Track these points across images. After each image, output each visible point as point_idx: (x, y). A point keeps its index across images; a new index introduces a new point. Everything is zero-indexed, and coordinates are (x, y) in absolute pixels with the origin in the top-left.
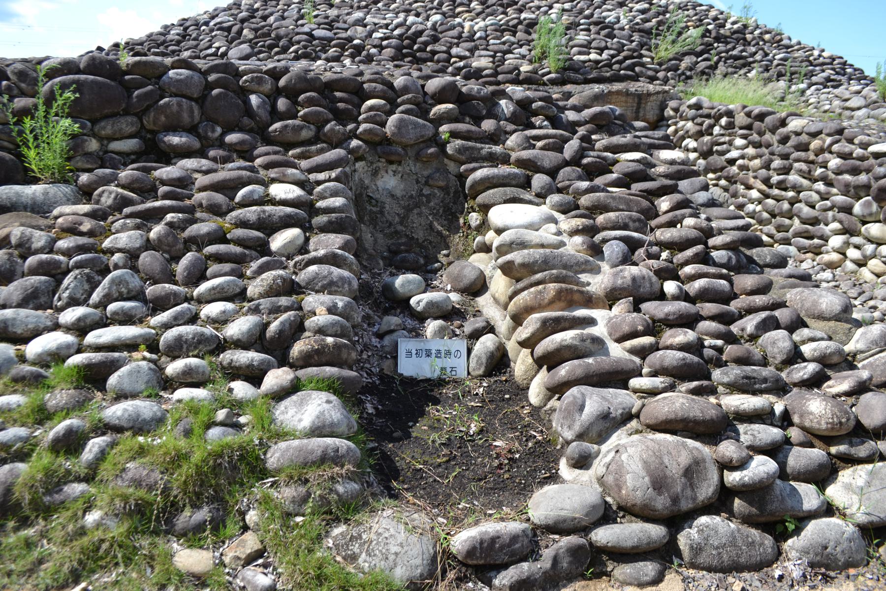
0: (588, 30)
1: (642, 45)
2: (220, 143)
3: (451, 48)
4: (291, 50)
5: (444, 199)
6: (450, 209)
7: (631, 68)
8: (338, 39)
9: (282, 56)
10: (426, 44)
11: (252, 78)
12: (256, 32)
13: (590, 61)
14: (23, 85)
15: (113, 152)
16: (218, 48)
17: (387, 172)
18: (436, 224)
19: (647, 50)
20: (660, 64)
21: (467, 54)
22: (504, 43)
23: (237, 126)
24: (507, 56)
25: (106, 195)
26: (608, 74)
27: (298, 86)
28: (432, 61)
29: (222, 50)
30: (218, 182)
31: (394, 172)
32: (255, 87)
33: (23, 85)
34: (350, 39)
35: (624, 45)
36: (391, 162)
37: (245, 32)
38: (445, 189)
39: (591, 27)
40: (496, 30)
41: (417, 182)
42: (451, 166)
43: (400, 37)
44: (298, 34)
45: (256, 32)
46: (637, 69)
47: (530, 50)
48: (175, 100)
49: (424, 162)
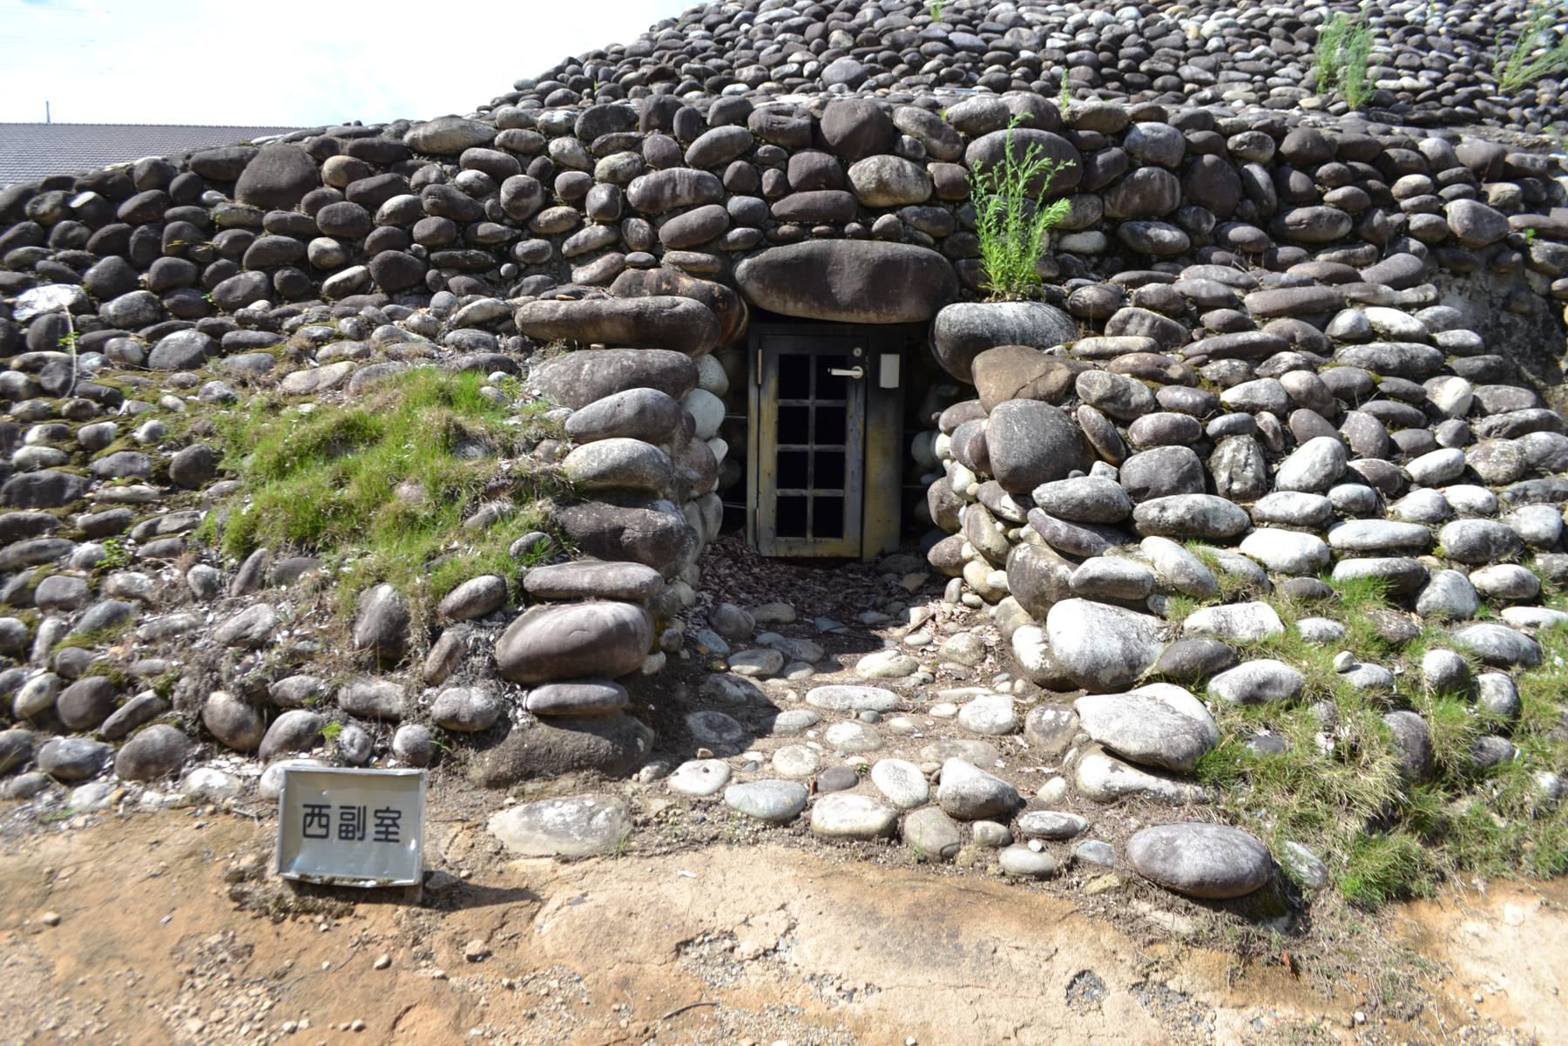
0: (1383, 35)
1: (1474, 61)
2: (1222, 242)
3: (1177, 66)
4: (927, 67)
5: (1529, 331)
6: (1541, 347)
7: (1468, 101)
8: (995, 49)
9: (914, 79)
10: (1138, 59)
11: (1252, 138)
12: (855, 36)
13: (1403, 89)
14: (936, 143)
15: (1069, 251)
16: (802, 64)
17: (1449, 289)
18: (1524, 369)
19: (1482, 70)
20: (1509, 95)
21: (1210, 76)
22: (1258, 57)
23: (1234, 213)
24: (1271, 81)
25: (1135, 320)
26: (1439, 113)
27: (1316, 152)
28: (1151, 88)
29: (809, 67)
30: (1302, 305)
31: (1460, 289)
32: (1255, 152)
33: (936, 143)
34: (1014, 51)
35: (1449, 63)
36: (1456, 274)
37: (836, 36)
38: (1529, 316)
39: (1389, 30)
40: (1239, 36)
41: (1492, 305)
42: (1537, 282)
43: (1092, 45)
44: (926, 40)
45: (855, 36)
46: (1479, 103)
47: (1303, 71)
48: (1156, 171)
49: (1498, 275)
